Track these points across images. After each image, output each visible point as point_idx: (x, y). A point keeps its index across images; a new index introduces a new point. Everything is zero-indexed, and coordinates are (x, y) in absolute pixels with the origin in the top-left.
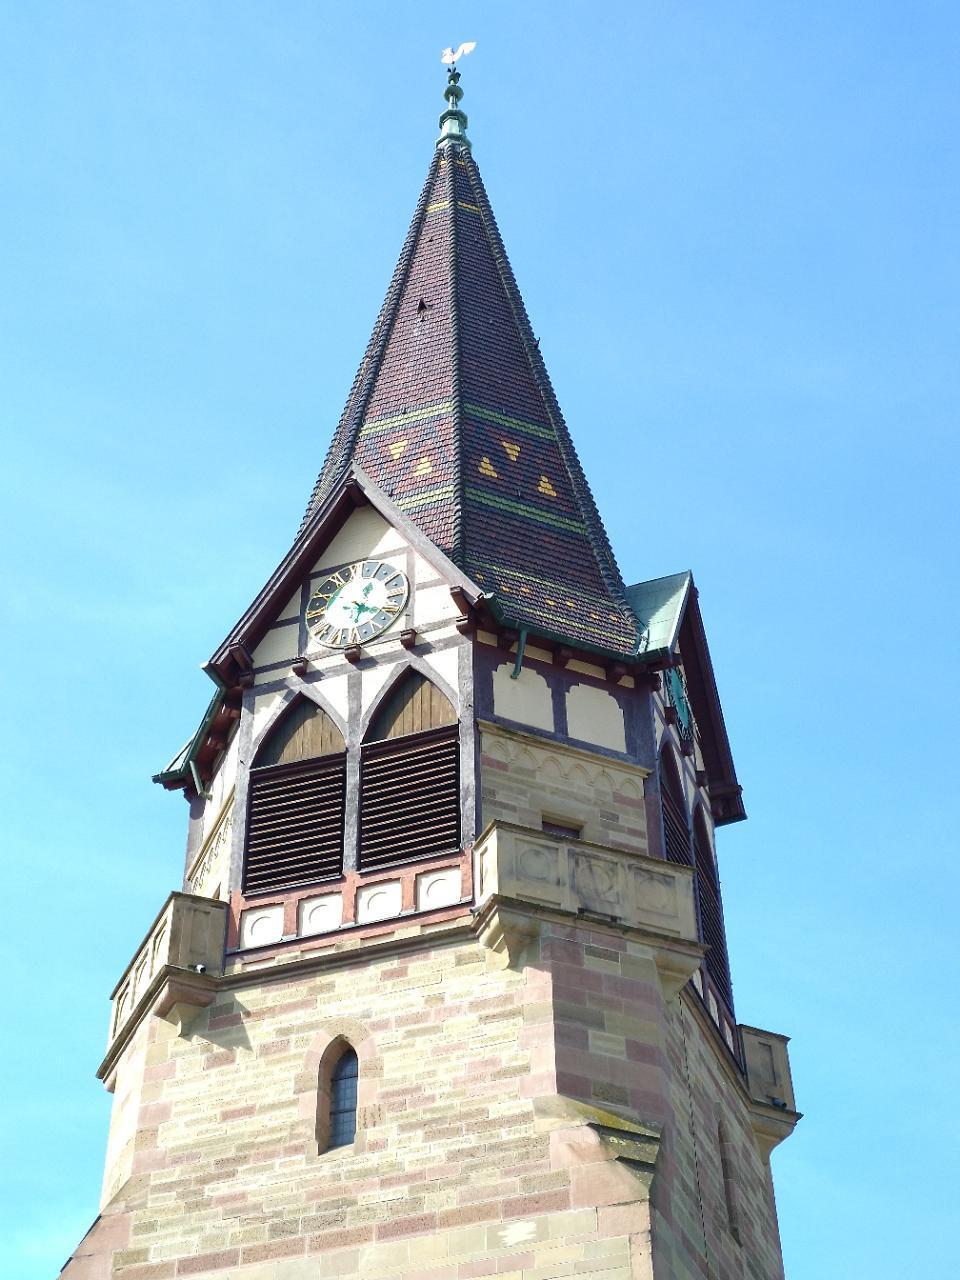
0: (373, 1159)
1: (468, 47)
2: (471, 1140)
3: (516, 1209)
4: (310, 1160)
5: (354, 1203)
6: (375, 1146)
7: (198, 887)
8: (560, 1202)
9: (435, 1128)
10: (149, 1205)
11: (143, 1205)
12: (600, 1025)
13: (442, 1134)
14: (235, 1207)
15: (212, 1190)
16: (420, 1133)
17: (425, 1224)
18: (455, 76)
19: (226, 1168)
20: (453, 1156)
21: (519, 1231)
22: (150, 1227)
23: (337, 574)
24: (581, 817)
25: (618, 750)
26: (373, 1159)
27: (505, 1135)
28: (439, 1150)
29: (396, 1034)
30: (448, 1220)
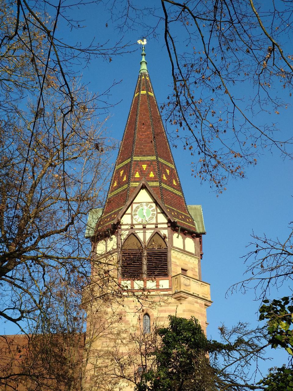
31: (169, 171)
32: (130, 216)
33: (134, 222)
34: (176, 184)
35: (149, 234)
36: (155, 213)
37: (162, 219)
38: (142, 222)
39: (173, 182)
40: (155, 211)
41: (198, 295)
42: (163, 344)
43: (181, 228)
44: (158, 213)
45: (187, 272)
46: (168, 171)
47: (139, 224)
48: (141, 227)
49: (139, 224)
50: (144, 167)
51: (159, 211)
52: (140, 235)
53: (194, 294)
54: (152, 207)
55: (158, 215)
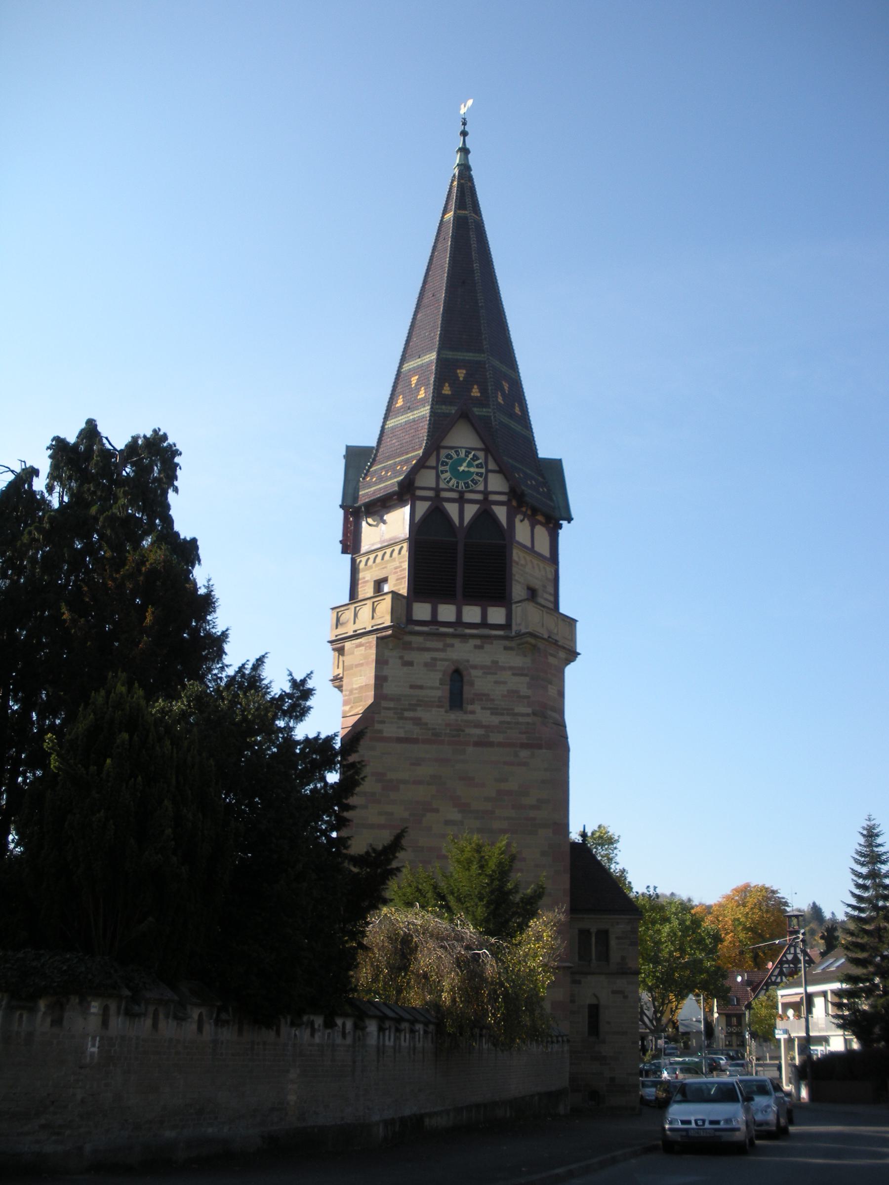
0: (470, 717)
1: (470, 103)
2: (508, 719)
3: (524, 746)
4: (446, 712)
5: (463, 731)
6: (473, 712)
7: (734, 1124)
8: (540, 747)
9: (495, 711)
10: (355, 653)
11: (452, 873)
12: (551, 683)
13: (497, 714)
14: (417, 721)
15: (407, 714)
16: (489, 712)
17: (491, 744)
18: (464, 119)
19: (412, 708)
20: (501, 722)
21: (524, 754)
22: (383, 722)
23: (453, 451)
24: (537, 587)
25: (526, 544)
26: (470, 717)
27: (521, 719)
28: (495, 720)
29: (479, 673)
30: (500, 745)
31: (507, 385)
32: (433, 472)
33: (442, 485)
34: (520, 413)
35: (471, 511)
36: (483, 470)
37: (496, 483)
38: (457, 487)
39: (509, 388)
40: (483, 468)
41: (365, 628)
42: (404, 1003)
43: (459, 209)
44: (488, 471)
45: (659, 894)
46: (506, 386)
47: (451, 490)
48: (454, 495)
49: (451, 490)
50: (461, 373)
51: (492, 465)
52: (452, 509)
53: (358, 632)
54: (478, 459)
55: (490, 475)
